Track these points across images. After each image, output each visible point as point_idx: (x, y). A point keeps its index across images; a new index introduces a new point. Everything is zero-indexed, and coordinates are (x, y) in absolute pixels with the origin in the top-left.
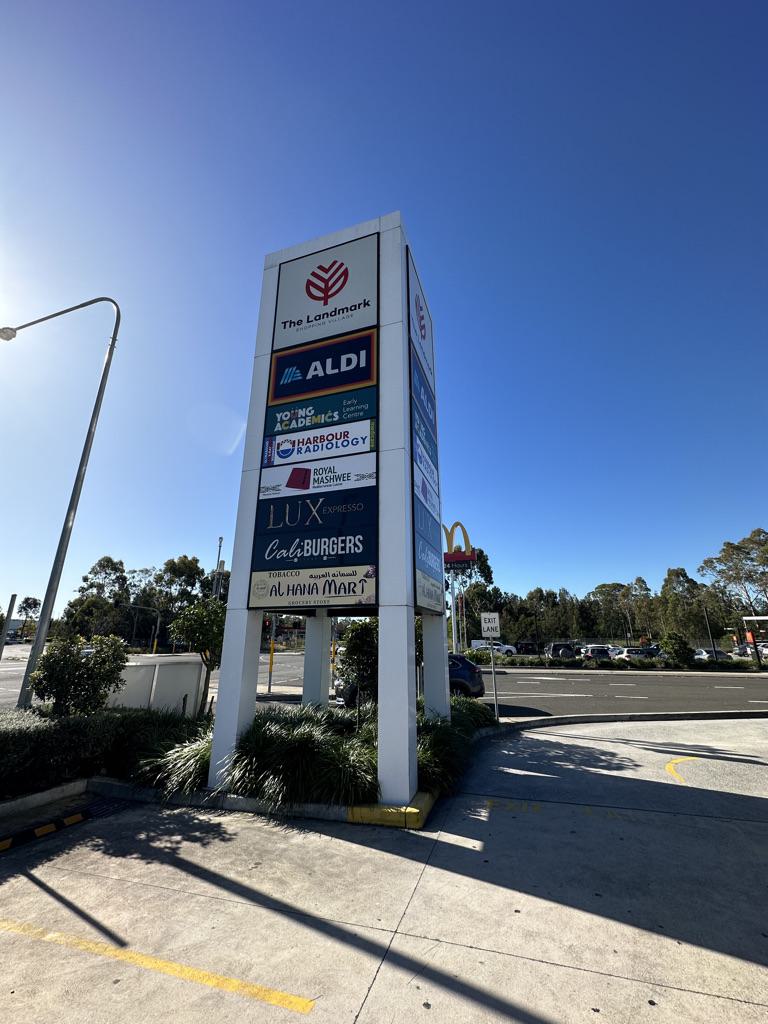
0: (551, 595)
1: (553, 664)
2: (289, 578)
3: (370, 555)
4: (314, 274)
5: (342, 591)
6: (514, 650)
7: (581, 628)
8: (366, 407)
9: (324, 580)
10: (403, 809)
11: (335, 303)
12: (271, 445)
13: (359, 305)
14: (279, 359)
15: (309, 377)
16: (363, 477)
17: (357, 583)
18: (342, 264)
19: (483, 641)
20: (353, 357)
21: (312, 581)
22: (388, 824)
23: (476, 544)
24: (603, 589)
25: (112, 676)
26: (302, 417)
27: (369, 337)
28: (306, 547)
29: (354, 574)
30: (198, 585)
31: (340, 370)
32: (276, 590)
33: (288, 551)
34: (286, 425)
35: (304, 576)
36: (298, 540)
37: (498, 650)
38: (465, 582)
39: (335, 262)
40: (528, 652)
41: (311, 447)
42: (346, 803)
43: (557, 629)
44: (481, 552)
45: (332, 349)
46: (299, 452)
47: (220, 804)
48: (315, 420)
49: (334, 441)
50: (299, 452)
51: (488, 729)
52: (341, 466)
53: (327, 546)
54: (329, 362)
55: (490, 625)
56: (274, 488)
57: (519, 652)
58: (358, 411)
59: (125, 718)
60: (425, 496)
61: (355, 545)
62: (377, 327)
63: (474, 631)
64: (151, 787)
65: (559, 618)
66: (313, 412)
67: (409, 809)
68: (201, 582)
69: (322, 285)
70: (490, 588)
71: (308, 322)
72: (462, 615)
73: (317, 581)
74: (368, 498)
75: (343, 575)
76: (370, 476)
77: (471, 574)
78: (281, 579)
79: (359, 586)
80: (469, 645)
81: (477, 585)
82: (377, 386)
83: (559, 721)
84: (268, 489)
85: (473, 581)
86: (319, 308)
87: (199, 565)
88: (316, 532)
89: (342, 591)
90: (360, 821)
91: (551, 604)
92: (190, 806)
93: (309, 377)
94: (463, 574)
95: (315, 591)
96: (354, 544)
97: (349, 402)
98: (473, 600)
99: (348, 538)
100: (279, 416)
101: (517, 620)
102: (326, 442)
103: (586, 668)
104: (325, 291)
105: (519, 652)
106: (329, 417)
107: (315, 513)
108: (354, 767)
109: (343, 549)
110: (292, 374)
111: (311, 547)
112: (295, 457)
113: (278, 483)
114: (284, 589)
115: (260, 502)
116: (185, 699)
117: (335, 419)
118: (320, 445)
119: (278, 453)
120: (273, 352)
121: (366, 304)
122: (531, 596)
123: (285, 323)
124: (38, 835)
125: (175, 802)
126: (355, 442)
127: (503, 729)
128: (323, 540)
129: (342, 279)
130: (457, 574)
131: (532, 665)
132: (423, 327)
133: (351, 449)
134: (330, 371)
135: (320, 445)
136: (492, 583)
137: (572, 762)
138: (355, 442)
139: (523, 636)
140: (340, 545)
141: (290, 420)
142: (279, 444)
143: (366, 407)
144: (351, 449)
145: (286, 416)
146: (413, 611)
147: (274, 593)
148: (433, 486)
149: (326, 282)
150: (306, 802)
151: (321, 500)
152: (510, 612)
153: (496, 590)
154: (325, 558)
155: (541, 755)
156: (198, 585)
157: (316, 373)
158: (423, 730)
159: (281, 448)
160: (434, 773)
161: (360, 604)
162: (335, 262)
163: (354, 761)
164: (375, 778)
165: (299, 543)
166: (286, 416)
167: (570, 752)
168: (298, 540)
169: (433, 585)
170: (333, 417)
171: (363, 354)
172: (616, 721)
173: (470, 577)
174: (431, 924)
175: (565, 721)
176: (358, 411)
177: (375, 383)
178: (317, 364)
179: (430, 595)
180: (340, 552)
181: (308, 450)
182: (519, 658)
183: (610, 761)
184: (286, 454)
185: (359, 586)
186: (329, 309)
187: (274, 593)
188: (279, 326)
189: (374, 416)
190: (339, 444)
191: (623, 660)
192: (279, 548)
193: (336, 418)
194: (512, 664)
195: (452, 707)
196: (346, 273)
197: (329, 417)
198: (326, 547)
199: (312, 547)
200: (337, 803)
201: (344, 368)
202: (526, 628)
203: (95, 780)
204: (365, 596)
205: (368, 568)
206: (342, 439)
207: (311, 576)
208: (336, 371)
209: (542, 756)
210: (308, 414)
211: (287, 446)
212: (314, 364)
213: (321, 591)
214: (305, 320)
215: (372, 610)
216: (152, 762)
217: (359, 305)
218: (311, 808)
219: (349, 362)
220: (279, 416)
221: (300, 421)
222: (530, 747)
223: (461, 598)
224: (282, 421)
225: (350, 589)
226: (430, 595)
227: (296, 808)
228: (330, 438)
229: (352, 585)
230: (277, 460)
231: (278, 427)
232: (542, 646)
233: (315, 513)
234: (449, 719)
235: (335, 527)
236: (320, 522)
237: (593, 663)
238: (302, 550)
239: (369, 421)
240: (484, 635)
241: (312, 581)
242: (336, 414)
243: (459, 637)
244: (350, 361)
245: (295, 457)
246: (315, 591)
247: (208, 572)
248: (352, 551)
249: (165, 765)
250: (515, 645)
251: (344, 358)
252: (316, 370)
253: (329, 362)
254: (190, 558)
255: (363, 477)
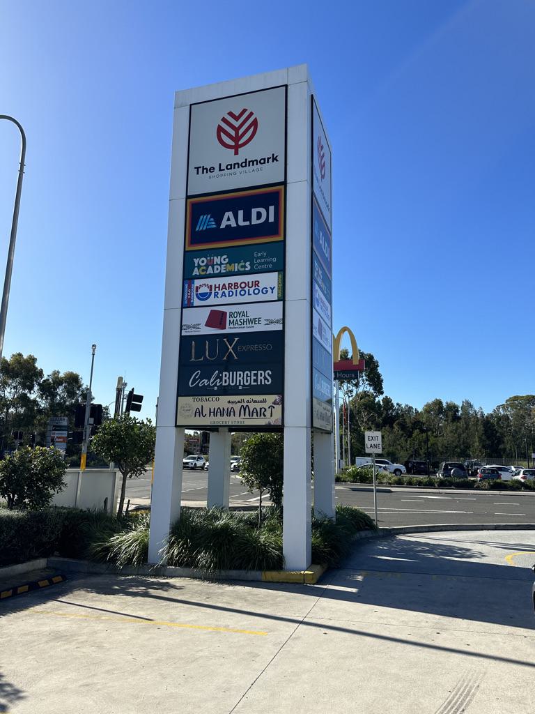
0: (452, 408)
1: (442, 484)
2: (210, 403)
3: (278, 387)
4: (224, 120)
5: (255, 414)
6: (403, 468)
7: (484, 447)
8: (274, 260)
9: (240, 405)
10: (302, 572)
11: (246, 153)
12: (190, 287)
13: (268, 159)
14: (193, 205)
15: (223, 226)
16: (272, 322)
17: (267, 408)
18: (251, 114)
19: (369, 459)
20: (263, 211)
21: (230, 406)
22: (291, 581)
23: (366, 351)
24: (514, 402)
25: (56, 481)
26: (217, 264)
27: (278, 193)
28: (224, 378)
29: (265, 401)
30: (36, 388)
31: (251, 222)
32: (199, 412)
33: (209, 381)
34: (203, 270)
35: (223, 401)
36: (217, 372)
37: (385, 468)
38: (351, 391)
39: (245, 111)
40: (419, 472)
41: (227, 292)
42: (260, 569)
43: (456, 447)
44: (371, 357)
45: (245, 200)
46: (216, 296)
47: (162, 573)
48: (230, 268)
49: (247, 289)
50: (216, 296)
51: (367, 532)
52: (253, 311)
53: (241, 378)
54: (241, 213)
55: (373, 442)
56: (194, 327)
57: (409, 471)
58: (268, 263)
59: (69, 513)
60: (321, 334)
61: (265, 378)
62: (284, 183)
63: (357, 449)
64: (105, 562)
65: (460, 435)
66: (227, 260)
67: (306, 572)
68: (39, 384)
69: (233, 133)
70: (380, 399)
71: (220, 170)
72: (346, 428)
73: (234, 406)
74: (275, 341)
75: (255, 402)
76: (277, 322)
77: (358, 383)
78: (203, 403)
79: (268, 411)
80: (353, 462)
81: (365, 394)
82: (284, 242)
83: (431, 529)
84: (189, 327)
85: (361, 390)
86: (228, 156)
87: (36, 365)
88: (230, 366)
89: (255, 414)
90: (271, 580)
91: (450, 418)
92: (138, 575)
93: (223, 226)
94: (349, 382)
95: (232, 414)
96: (264, 377)
97: (259, 255)
98: (359, 412)
99: (259, 372)
100: (196, 261)
101: (410, 436)
102: (240, 289)
103: (478, 488)
104: (236, 139)
105: (409, 471)
106: (242, 267)
107: (231, 350)
108: (264, 545)
109: (256, 381)
110: (206, 222)
111: (228, 378)
112: (212, 300)
113: (198, 321)
114: (206, 411)
115: (182, 338)
116: (106, 502)
117: (247, 269)
118: (234, 291)
119: (197, 295)
120: (188, 197)
121: (275, 159)
122: (428, 409)
123: (198, 168)
124: (41, 586)
125: (124, 572)
126: (265, 291)
127: (381, 534)
128: (238, 373)
129: (253, 128)
130: (342, 383)
131: (420, 484)
132: (323, 166)
133: (261, 297)
134: (242, 223)
135: (234, 291)
136: (382, 393)
137: (434, 553)
138: (265, 291)
139: (416, 453)
140: (253, 378)
141: (207, 266)
142: (197, 287)
143: (274, 260)
144: (261, 297)
145: (203, 262)
146: (310, 430)
147: (197, 414)
148: (326, 319)
149: (236, 130)
150: (230, 569)
151: (236, 339)
152: (403, 426)
153: (387, 401)
154: (240, 388)
155: (410, 549)
156: (36, 388)
157: (228, 223)
158: (315, 526)
159: (200, 291)
160: (324, 552)
161: (269, 425)
162: (245, 111)
163: (264, 542)
164: (282, 553)
165: (219, 374)
166: (203, 262)
167: (433, 548)
168: (217, 372)
169: (325, 409)
170: (245, 267)
171: (272, 208)
172: (482, 530)
173: (357, 385)
174: (327, 615)
175: (436, 529)
176: (268, 263)
177: (281, 238)
178: (230, 214)
179: (322, 417)
180: (252, 383)
181: (224, 295)
182: (407, 477)
183: (465, 552)
184: (204, 297)
185: (268, 411)
186: (240, 159)
187: (197, 414)
188: (193, 171)
189: (281, 268)
190: (251, 292)
191: (518, 482)
192: (201, 378)
193: (248, 268)
194: (399, 483)
195: (337, 513)
196: (255, 123)
197: (242, 267)
198: (241, 379)
199: (229, 378)
200: (253, 569)
201: (254, 221)
202: (420, 445)
203: (53, 559)
204: (274, 419)
205: (276, 397)
206: (254, 288)
207: (229, 402)
208: (247, 223)
209: (411, 550)
210: (223, 262)
211: (204, 290)
212: (227, 214)
213: (237, 414)
214: (217, 168)
215: (279, 429)
216: (100, 546)
217: (268, 159)
218: (234, 573)
219: (259, 215)
220: (196, 261)
221: (215, 267)
222: (401, 545)
223: (346, 409)
224: (199, 266)
225: (261, 413)
226: (322, 417)
227: (223, 573)
228: (243, 285)
229: (263, 410)
230: (196, 302)
231: (196, 272)
232: (436, 465)
233: (231, 350)
234: (334, 519)
235: (247, 363)
236: (236, 358)
237: (485, 484)
238: (221, 380)
239: (277, 273)
240: (367, 451)
241: (230, 406)
242: (248, 264)
243: (341, 453)
244: (261, 215)
245: (212, 300)
246: (232, 414)
247: (47, 374)
248: (263, 383)
249: (112, 546)
250: (406, 464)
251: (254, 211)
252: (228, 220)
253: (241, 213)
254: (25, 357)
255: (272, 322)
